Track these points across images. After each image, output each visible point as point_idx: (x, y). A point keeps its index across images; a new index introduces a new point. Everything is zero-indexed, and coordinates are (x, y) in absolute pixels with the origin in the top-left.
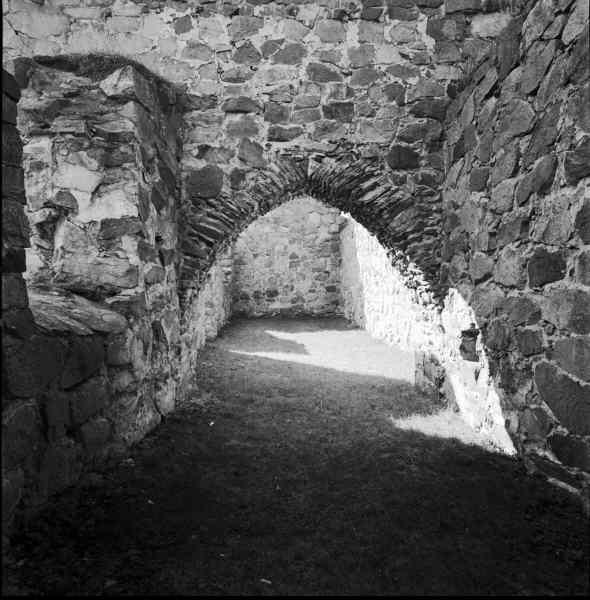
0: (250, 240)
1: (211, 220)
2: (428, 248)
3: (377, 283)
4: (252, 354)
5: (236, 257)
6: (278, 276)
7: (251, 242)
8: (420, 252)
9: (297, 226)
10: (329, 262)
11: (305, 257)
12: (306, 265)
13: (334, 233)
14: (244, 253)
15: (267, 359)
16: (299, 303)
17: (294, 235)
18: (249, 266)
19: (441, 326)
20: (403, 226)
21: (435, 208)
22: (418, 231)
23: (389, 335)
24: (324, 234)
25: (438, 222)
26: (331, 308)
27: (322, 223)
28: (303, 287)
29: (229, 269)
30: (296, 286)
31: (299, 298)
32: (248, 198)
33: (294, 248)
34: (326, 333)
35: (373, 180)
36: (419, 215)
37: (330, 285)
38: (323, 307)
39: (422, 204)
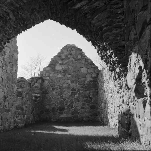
0: (51, 81)
5: (43, 90)
6: (65, 99)
7: (51, 82)
11: (79, 90)
13: (94, 78)
14: (48, 88)
17: (74, 79)
18: (50, 94)
21: (120, 12)
22: (110, 25)
24: (89, 78)
28: (78, 105)
29: (39, 95)
31: (76, 111)
33: (73, 85)
39: (112, 10)
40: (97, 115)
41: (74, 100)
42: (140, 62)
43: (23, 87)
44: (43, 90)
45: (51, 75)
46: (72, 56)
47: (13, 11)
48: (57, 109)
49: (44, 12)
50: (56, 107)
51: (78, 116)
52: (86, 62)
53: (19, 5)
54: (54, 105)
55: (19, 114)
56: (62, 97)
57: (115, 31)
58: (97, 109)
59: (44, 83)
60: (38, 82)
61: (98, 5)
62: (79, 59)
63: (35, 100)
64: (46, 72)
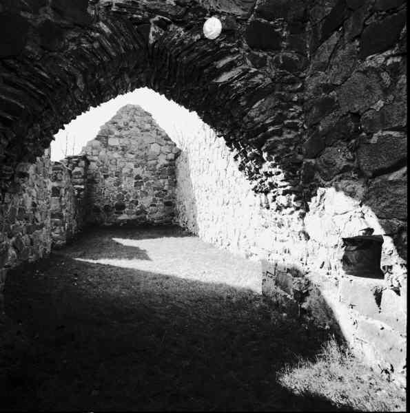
0: (101, 163)
1: (9, 89)
2: (289, 142)
3: (207, 197)
4: (95, 262)
5: (89, 177)
6: (126, 193)
7: (102, 165)
8: (280, 147)
9: (142, 154)
10: (167, 183)
11: (147, 179)
12: (148, 184)
13: (171, 160)
14: (96, 174)
15: (109, 266)
16: (143, 215)
17: (139, 161)
18: (100, 185)
19: (304, 233)
20: (261, 116)
21: (296, 98)
22: (278, 124)
23: (219, 240)
24: (162, 161)
25: (300, 114)
26: (168, 218)
27: (161, 152)
28: (146, 202)
29: (83, 187)
30: (139, 201)
32: (66, 66)
33: (138, 171)
34: (165, 239)
35: (229, 59)
36: (279, 106)
37: (167, 200)
38: (162, 218)
40: (174, 216)
41: (139, 194)
42: (365, 217)
43: (59, 178)
44: (89, 177)
45: (101, 153)
46: (135, 125)
47: (84, 73)
48: (113, 207)
49: (142, 75)
50: (111, 204)
51: (145, 217)
52: (157, 134)
53: (99, 59)
54: (108, 201)
55: (56, 224)
56: (121, 189)
57: (288, 135)
58: (174, 207)
59: (90, 167)
60: (80, 164)
61: (261, 81)
62: (148, 131)
63: (78, 196)
64: (93, 148)
